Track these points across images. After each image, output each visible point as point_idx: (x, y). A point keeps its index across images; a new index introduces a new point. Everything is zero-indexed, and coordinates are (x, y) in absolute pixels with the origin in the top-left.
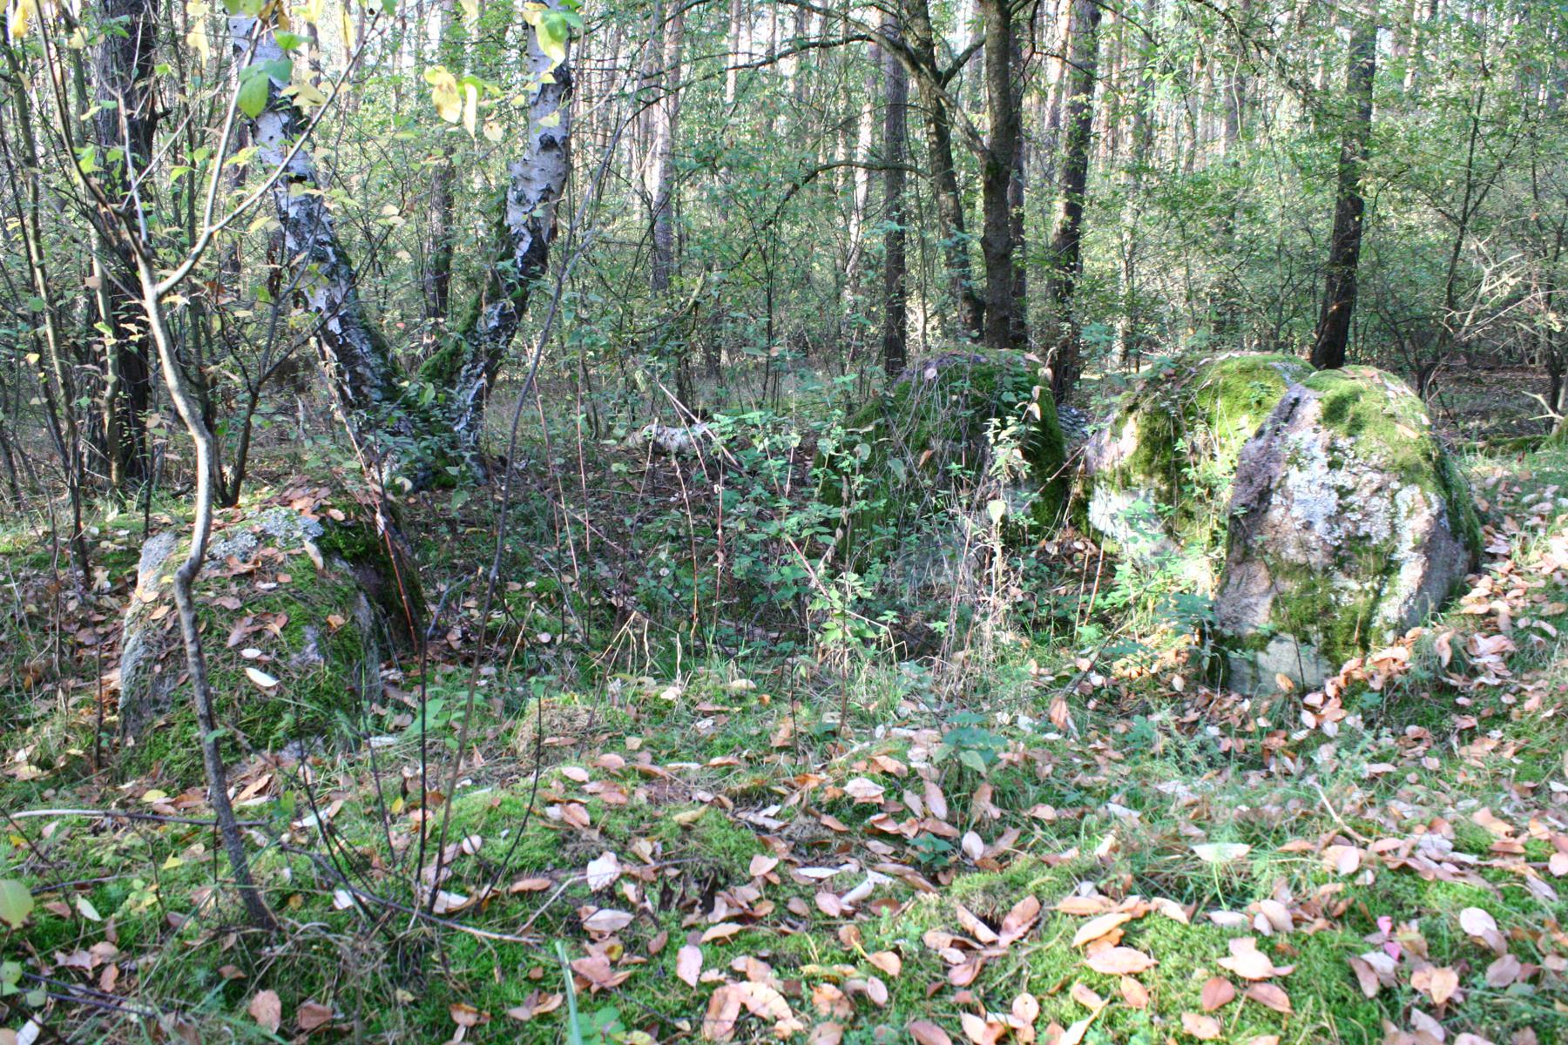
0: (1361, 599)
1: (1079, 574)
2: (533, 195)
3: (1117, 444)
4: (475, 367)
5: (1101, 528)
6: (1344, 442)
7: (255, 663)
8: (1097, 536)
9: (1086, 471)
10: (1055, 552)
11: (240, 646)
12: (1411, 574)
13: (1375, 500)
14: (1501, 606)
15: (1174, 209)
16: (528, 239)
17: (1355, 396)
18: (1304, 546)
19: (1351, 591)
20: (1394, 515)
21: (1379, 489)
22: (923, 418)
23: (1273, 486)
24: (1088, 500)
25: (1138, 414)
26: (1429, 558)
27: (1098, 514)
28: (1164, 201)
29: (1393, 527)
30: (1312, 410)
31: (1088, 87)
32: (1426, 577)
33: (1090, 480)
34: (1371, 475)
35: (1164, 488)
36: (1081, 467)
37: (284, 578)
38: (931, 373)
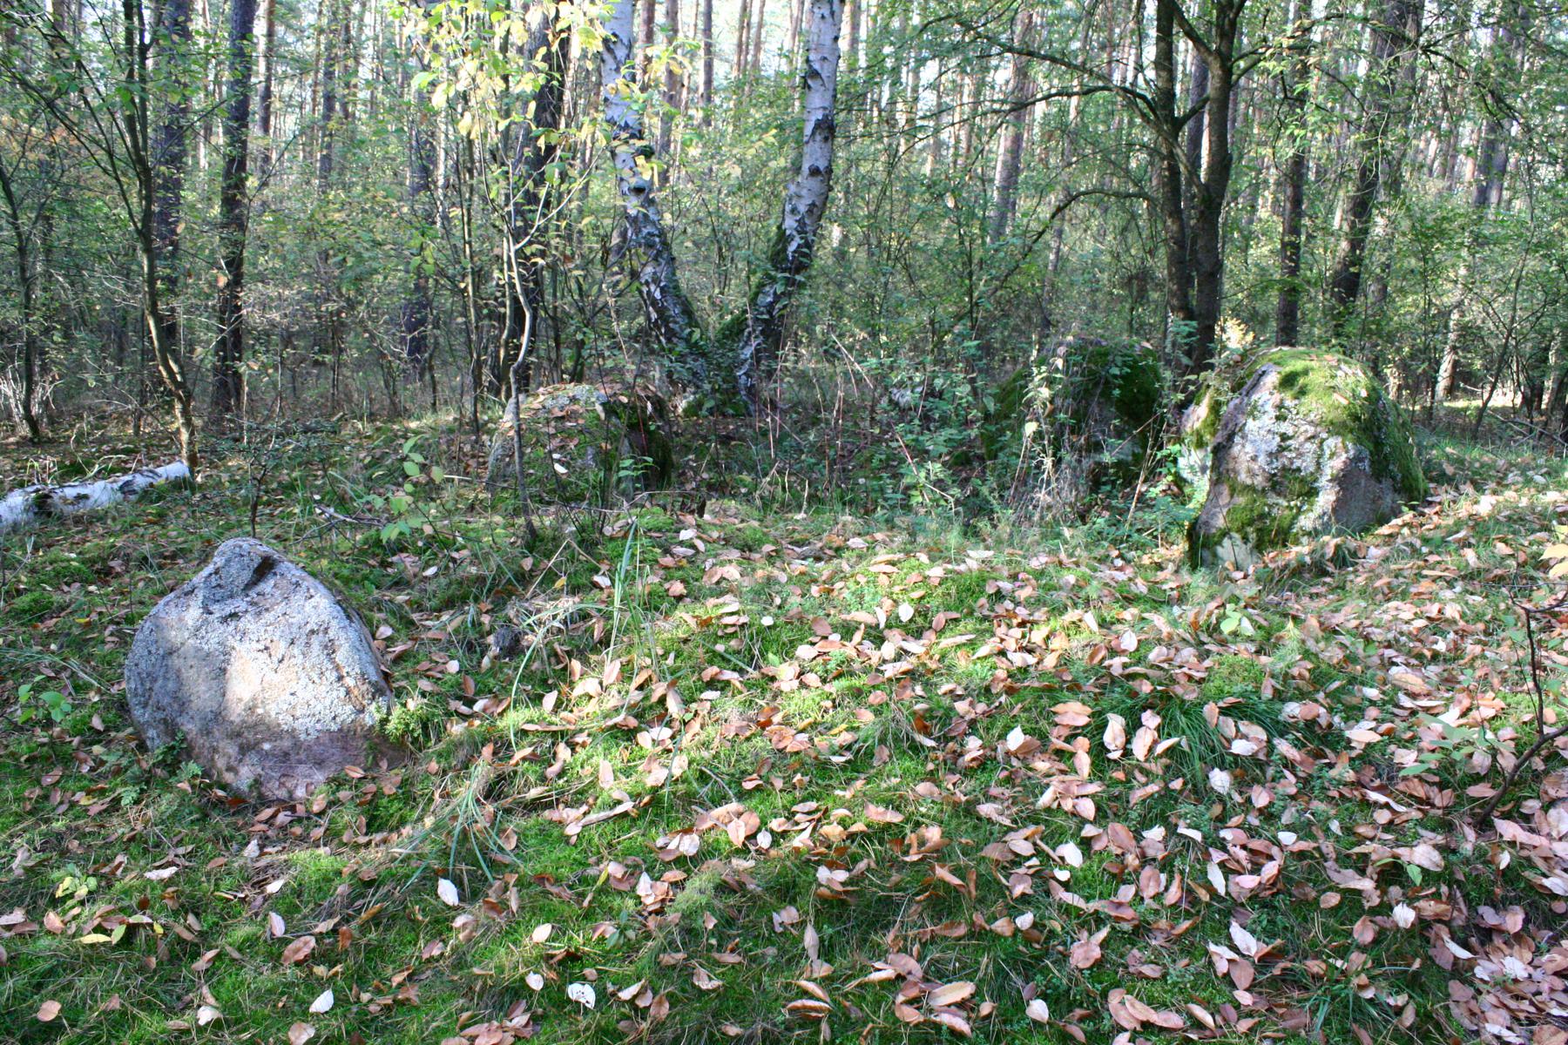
0: (1287, 512)
2: (803, 208)
6: (1289, 403)
7: (559, 461)
12: (1326, 498)
13: (1308, 445)
17: (1306, 372)
18: (1253, 475)
19: (1280, 506)
20: (1320, 456)
21: (1313, 437)
29: (1318, 464)
37: (581, 422)
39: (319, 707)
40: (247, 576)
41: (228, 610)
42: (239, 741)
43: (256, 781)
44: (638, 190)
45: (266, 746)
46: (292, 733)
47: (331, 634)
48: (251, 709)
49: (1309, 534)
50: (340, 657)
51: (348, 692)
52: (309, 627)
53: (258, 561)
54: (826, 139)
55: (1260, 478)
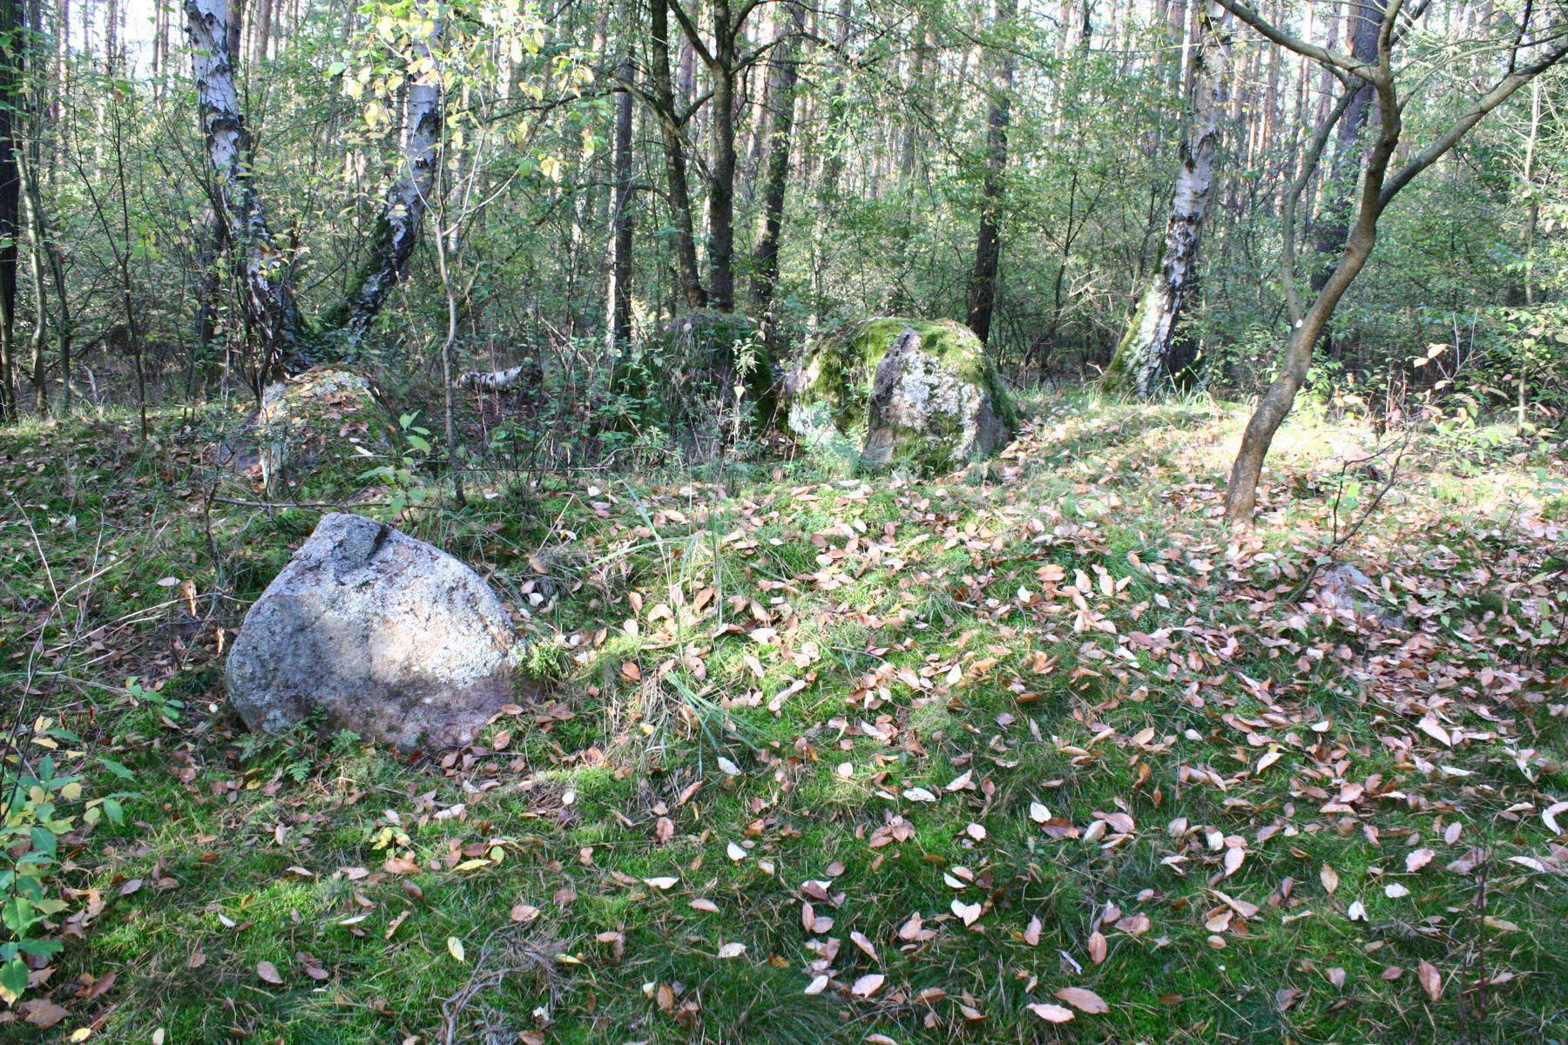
3: (807, 374)
6: (935, 359)
8: (793, 435)
11: (347, 436)
12: (969, 434)
14: (1021, 455)
16: (403, 230)
18: (913, 419)
25: (820, 355)
27: (795, 420)
30: (916, 341)
31: (787, 129)
32: (978, 437)
33: (791, 397)
38: (688, 326)
39: (472, 656)
40: (369, 545)
41: (360, 580)
42: (400, 700)
44: (247, 181)
45: (428, 700)
46: (450, 684)
47: (471, 589)
48: (407, 669)
50: (482, 608)
51: (493, 640)
52: (447, 586)
53: (377, 531)
54: (432, 133)
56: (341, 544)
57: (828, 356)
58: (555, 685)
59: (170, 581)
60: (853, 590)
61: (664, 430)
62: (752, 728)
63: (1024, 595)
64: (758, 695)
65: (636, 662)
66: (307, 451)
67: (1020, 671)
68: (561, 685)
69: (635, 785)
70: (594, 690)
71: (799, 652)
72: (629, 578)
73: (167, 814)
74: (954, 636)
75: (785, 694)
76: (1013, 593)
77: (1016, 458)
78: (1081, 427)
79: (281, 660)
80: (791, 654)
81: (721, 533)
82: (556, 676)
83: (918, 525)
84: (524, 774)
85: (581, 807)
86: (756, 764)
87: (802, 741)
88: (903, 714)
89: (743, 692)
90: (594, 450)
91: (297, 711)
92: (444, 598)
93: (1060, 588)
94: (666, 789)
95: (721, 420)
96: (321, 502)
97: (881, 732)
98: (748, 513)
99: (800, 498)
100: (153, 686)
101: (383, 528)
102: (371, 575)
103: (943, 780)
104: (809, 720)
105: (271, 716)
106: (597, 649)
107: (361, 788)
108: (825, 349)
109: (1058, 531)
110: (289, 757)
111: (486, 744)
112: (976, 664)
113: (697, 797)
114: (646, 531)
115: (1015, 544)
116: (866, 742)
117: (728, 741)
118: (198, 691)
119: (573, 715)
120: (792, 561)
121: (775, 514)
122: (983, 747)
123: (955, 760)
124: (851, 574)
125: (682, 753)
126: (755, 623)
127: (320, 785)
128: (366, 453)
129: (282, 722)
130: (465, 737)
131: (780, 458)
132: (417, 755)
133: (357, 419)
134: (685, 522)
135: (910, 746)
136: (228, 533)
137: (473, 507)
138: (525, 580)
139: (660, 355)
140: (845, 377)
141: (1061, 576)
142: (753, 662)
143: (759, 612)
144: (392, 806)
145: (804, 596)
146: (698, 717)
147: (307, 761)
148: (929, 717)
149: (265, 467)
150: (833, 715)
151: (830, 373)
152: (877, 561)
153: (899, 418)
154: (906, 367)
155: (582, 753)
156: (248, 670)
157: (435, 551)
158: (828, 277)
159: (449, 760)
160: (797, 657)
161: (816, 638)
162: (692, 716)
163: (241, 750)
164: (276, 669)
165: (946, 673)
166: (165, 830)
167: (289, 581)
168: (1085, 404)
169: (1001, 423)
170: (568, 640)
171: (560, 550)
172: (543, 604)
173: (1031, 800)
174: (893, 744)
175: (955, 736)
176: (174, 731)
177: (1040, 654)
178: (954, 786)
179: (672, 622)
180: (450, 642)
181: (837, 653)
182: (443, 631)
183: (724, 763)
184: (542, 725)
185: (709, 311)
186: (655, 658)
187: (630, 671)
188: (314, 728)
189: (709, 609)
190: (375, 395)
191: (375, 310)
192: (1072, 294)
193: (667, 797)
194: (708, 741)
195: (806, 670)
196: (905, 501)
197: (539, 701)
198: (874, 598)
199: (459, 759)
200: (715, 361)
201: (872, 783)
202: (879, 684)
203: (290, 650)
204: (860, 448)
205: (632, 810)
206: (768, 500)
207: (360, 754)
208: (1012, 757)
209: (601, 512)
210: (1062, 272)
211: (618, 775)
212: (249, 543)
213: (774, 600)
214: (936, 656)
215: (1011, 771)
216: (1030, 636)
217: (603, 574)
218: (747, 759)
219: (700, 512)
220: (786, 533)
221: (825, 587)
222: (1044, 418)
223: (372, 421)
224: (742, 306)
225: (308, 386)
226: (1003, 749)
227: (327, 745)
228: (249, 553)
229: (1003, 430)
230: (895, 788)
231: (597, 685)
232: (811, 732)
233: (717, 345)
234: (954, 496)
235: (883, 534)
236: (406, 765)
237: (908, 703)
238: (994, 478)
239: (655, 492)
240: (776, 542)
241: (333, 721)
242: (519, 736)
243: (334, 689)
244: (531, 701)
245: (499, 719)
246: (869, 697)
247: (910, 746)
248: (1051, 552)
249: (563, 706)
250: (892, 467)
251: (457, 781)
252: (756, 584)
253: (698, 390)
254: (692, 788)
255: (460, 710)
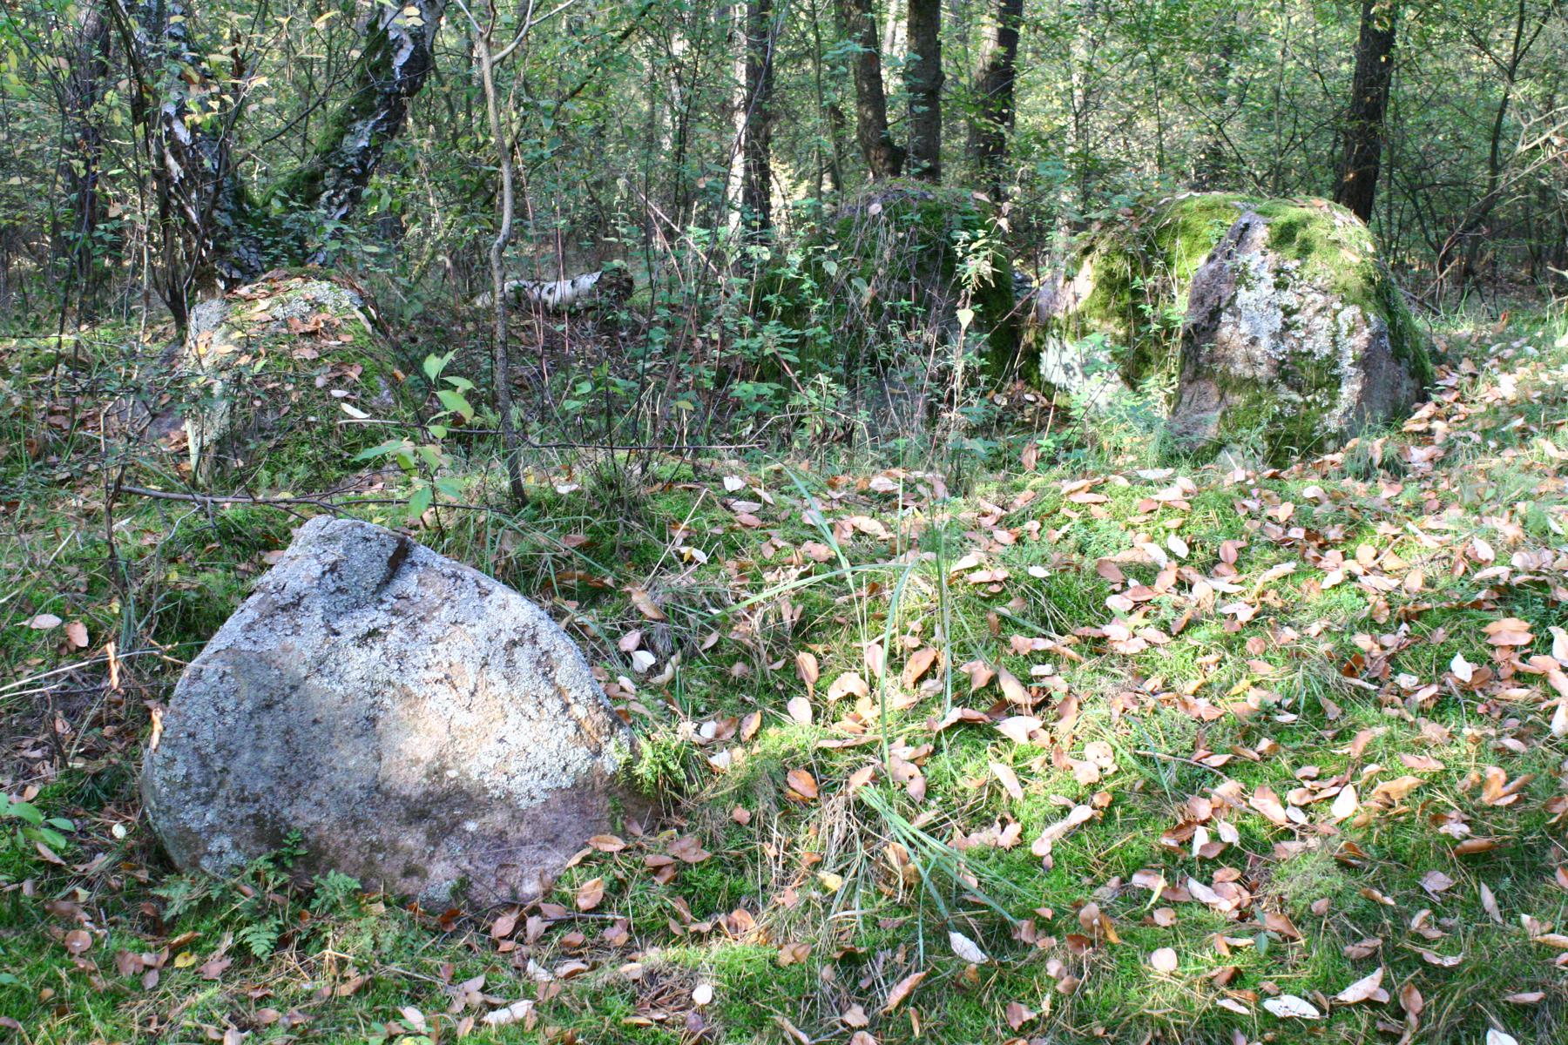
1: (1031, 424)
3: (1072, 285)
4: (336, 195)
5: (1053, 381)
6: (1292, 265)
8: (1048, 389)
9: (1036, 320)
10: (1005, 403)
11: (327, 387)
12: (1349, 391)
13: (1318, 320)
15: (1144, 40)
17: (1305, 222)
18: (1250, 360)
21: (1323, 309)
22: (867, 256)
23: (1223, 305)
24: (1040, 350)
25: (1095, 256)
26: (1368, 375)
28: (1129, 29)
29: (1335, 343)
30: (1261, 234)
32: (1365, 395)
34: (1315, 295)
35: (1121, 332)
36: (1033, 314)
37: (347, 339)
38: (876, 208)
39: (543, 755)
40: (378, 570)
41: (364, 626)
42: (426, 825)
43: (462, 882)
46: (507, 800)
47: (544, 642)
48: (437, 773)
49: (1335, 437)
50: (562, 675)
52: (504, 638)
55: (1264, 368)
56: (333, 568)
57: (1108, 257)
58: (677, 803)
59: (48, 621)
60: (1171, 656)
61: (837, 379)
62: (1005, 885)
63: (1462, 669)
64: (1013, 829)
65: (809, 769)
66: (263, 410)
67: (1458, 800)
68: (686, 804)
69: (813, 976)
70: (742, 814)
71: (1080, 758)
72: (797, 629)
73: (46, 1006)
74: (1342, 736)
75: (1058, 828)
76: (1443, 665)
77: (1430, 432)
78: (1544, 377)
79: (234, 755)
80: (1067, 760)
81: (949, 557)
82: (679, 790)
83: (1275, 546)
84: (627, 952)
85: (723, 1010)
86: (1013, 945)
87: (1091, 910)
88: (1259, 867)
89: (988, 822)
90: (720, 410)
91: (258, 839)
92: (499, 660)
93: (1525, 658)
94: (864, 984)
95: (933, 364)
96: (287, 495)
97: (1223, 897)
98: (987, 522)
99: (1077, 499)
100: (21, 793)
101: (402, 542)
102: (382, 619)
103: (1332, 983)
104: (1099, 873)
105: (214, 847)
106: (744, 744)
107: (361, 968)
108: (1103, 246)
109: (1517, 560)
110: (245, 916)
111: (563, 900)
112: (1382, 786)
113: (915, 999)
114: (821, 551)
115: (1443, 582)
116: (1198, 913)
117: (965, 905)
118: (93, 803)
119: (707, 854)
120: (1067, 606)
121: (1033, 525)
122: (1401, 928)
123: (1352, 950)
124: (1165, 628)
125: (890, 923)
126: (1006, 708)
127: (293, 963)
128: (358, 414)
129: (233, 857)
130: (530, 888)
131: (1027, 427)
132: (451, 915)
133: (343, 360)
134: (884, 535)
135: (1273, 923)
136: (135, 543)
137: (538, 506)
138: (626, 629)
139: (833, 256)
140: (1137, 293)
141: (1525, 639)
142: (1004, 773)
143: (1012, 690)
144: (414, 1000)
145: (1087, 664)
146: (916, 863)
147: (273, 922)
148: (1304, 872)
149: (192, 435)
150: (1140, 865)
151: (1111, 287)
152: (1208, 606)
153: (1232, 361)
154: (1242, 278)
155: (722, 919)
156: (180, 770)
157: (487, 582)
158: (1100, 123)
159: (504, 925)
160: (1077, 765)
161: (1109, 735)
162: (904, 863)
163: (164, 902)
164: (225, 770)
165: (1331, 799)
166: (43, 1033)
167: (250, 627)
168: (1549, 338)
169: (1405, 372)
170: (697, 730)
171: (682, 580)
172: (656, 669)
173: (1487, 1026)
174: (1242, 918)
175: (1350, 909)
176: (56, 868)
177: (1494, 772)
178: (1353, 993)
179: (868, 702)
180: (507, 730)
181: (1144, 760)
182: (497, 713)
183: (959, 941)
184: (657, 870)
185: (908, 183)
186: (842, 762)
187: (801, 783)
188: (284, 868)
189: (929, 684)
190: (371, 320)
191: (362, 179)
192: (1521, 148)
193: (865, 997)
194: (936, 904)
195: (1093, 788)
196: (1253, 505)
197: (651, 831)
198: (1204, 669)
199: (521, 924)
200: (920, 266)
201: (1210, 983)
202: (1216, 817)
203: (247, 741)
204: (1163, 412)
205: (810, 1017)
206: (1020, 501)
207: (360, 913)
208: (1452, 949)
209: (746, 519)
210: (1502, 112)
211: (785, 958)
212: (173, 560)
213: (1036, 670)
214: (1312, 771)
215: (1451, 971)
216: (1476, 740)
217: (756, 621)
218: (997, 936)
219: (909, 520)
220: (1055, 557)
221: (1122, 649)
222: (1479, 364)
223: (368, 361)
224: (953, 172)
225: (264, 304)
226: (1434, 933)
227: (306, 897)
228: (174, 577)
229: (1407, 384)
230: (1249, 993)
231: (747, 805)
232: (1105, 893)
233: (924, 239)
234: (1335, 499)
235: (1217, 561)
236: (435, 932)
237: (1266, 849)
238: (1395, 469)
239: (833, 486)
240: (1039, 572)
241: (316, 858)
242: (618, 888)
243: (319, 804)
244: (638, 831)
245: (587, 859)
246: (1201, 837)
247: (1273, 923)
248: (1507, 596)
249: (689, 840)
250: (1220, 447)
251: (517, 961)
252: (1006, 642)
253: (893, 313)
254: (908, 983)
255: (523, 843)
